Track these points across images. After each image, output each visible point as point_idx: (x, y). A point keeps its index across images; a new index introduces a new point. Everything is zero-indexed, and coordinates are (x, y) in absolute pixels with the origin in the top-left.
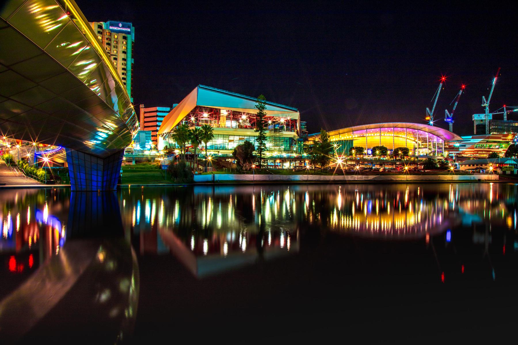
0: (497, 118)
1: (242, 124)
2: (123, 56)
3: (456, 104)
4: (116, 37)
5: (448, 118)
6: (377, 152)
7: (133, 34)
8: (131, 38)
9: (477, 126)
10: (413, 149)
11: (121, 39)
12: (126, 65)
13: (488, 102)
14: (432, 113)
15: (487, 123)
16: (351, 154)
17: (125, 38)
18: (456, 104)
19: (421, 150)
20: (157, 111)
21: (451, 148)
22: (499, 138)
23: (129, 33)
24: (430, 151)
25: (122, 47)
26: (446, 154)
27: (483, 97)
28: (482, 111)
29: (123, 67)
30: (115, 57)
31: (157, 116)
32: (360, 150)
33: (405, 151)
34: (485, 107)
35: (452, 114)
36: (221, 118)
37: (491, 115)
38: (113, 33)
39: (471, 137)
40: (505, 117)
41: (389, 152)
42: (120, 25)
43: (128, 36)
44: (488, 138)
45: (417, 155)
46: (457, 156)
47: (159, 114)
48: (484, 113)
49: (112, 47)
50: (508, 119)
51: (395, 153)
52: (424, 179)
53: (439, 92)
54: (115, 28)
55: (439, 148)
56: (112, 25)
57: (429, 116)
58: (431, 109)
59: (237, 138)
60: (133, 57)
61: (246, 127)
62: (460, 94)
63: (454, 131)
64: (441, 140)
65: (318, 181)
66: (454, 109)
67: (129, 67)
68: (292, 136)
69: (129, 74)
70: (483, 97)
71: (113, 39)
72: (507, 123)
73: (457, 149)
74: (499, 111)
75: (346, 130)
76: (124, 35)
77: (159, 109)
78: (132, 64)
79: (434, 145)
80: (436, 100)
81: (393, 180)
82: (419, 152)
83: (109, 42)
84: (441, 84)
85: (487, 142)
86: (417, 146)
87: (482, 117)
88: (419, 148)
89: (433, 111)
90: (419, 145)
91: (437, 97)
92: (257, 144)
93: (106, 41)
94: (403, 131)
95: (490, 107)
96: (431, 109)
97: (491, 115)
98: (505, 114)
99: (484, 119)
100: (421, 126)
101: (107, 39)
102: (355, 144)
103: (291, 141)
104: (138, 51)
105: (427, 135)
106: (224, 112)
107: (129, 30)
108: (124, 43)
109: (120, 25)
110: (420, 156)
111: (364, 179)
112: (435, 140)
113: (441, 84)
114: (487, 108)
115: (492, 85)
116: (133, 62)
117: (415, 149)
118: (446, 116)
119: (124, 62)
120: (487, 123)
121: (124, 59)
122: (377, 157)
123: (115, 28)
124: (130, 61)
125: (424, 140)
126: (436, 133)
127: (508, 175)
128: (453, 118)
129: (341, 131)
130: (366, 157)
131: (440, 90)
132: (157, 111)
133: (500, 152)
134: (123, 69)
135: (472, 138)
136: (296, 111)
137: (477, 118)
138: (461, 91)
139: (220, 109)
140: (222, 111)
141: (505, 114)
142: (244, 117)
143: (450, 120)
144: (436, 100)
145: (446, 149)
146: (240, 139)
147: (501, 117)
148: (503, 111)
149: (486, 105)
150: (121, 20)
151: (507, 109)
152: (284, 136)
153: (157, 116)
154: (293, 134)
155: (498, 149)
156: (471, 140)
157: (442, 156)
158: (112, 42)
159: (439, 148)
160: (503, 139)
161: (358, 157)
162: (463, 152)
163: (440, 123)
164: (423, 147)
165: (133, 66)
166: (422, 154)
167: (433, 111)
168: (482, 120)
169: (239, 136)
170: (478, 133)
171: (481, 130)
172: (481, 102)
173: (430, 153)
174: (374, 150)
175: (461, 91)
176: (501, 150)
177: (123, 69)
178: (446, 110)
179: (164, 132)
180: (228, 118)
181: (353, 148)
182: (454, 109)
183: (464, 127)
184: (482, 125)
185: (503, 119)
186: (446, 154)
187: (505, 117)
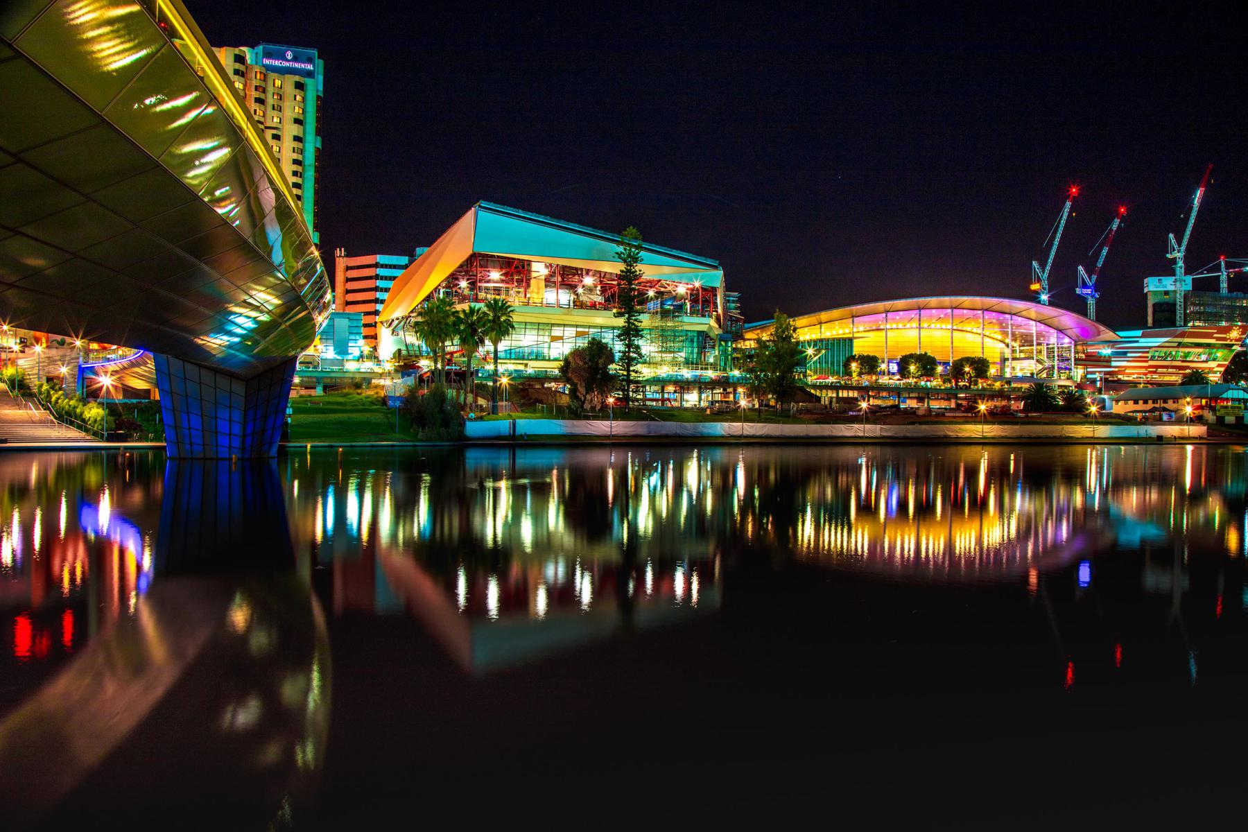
0: (1204, 287)
1: (584, 298)
2: (295, 130)
3: (1105, 251)
4: (278, 83)
5: (1085, 286)
6: (912, 368)
7: (321, 78)
8: (315, 86)
9: (1154, 305)
10: (998, 360)
11: (289, 89)
12: (302, 152)
13: (1183, 248)
14: (1046, 275)
15: (1180, 300)
16: (848, 373)
17: (300, 86)
18: (1105, 251)
19: (1017, 364)
20: (377, 265)
21: (1092, 360)
22: (1209, 336)
23: (310, 74)
24: (1040, 367)
25: (292, 109)
26: (1078, 373)
27: (1171, 236)
28: (1167, 269)
29: (295, 156)
30: (274, 132)
31: (377, 277)
32: (870, 363)
33: (980, 366)
34: (1174, 261)
35: (1094, 277)
36: (533, 282)
37: (1189, 279)
38: (272, 75)
39: (1139, 333)
40: (1224, 285)
41: (940, 369)
42: (289, 55)
43: (308, 81)
44: (1183, 335)
45: (1008, 375)
46: (1106, 380)
47: (382, 272)
48: (1173, 273)
49: (269, 108)
50: (1230, 289)
51: (957, 370)
52: (1025, 434)
53: (1063, 222)
54: (277, 63)
55: (1063, 359)
56: (268, 55)
57: (1039, 280)
58: (1043, 266)
59: (570, 332)
60: (318, 133)
61: (593, 306)
62: (1115, 227)
63: (1101, 319)
64: (1067, 340)
65: (761, 437)
66: (1100, 264)
67: (310, 158)
68: (704, 328)
69: (310, 174)
70: (1171, 236)
71: (270, 90)
72: (1227, 299)
73: (1106, 361)
74: (1209, 271)
75: (836, 313)
76: (297, 78)
77: (381, 259)
78: (317, 150)
79: (1050, 351)
80: (1056, 243)
81: (950, 437)
82: (1013, 368)
83: (262, 96)
84: (1068, 204)
85: (1180, 345)
86: (1008, 354)
87: (1168, 283)
88: (1014, 359)
89: (1048, 268)
90: (1013, 351)
91: (1059, 235)
92: (618, 347)
93: (255, 94)
94: (975, 318)
95: (1186, 260)
96: (1043, 266)
97: (1189, 279)
98: (1224, 276)
99: (1172, 288)
100: (1019, 305)
101: (257, 88)
102: (859, 348)
103: (704, 340)
104: (332, 117)
105: (1033, 328)
106: (539, 269)
107: (310, 67)
108: (298, 98)
109: (289, 55)
110: (1016, 379)
111: (878, 434)
112: (1053, 340)
113: (1068, 204)
114: (1180, 263)
115: (1191, 208)
116: (319, 146)
117: (1004, 360)
118: (1080, 282)
119: (296, 145)
120: (1180, 300)
121: (297, 139)
122: (911, 380)
123: (277, 63)
124: (312, 143)
125: (1027, 340)
126: (1055, 322)
127: (1229, 426)
128: (1096, 287)
129: (824, 316)
130: (884, 380)
131: (1065, 217)
132: (377, 265)
133: (1211, 370)
134: (296, 162)
135: (1143, 336)
136: (715, 267)
137: (1154, 286)
138: (1117, 222)
139: (529, 262)
140: (535, 266)
141: (1224, 276)
142: (589, 281)
143: (1089, 291)
144: (1056, 243)
145: (1078, 361)
146: (579, 335)
147: (1213, 285)
148: (1219, 270)
149: (1178, 254)
150: (290, 43)
151: (1228, 266)
152: (686, 328)
153: (377, 277)
154: (708, 323)
155: (1206, 362)
156: (1141, 340)
157: (1069, 378)
158: (270, 95)
159: (1063, 359)
160: (1218, 339)
161: (866, 380)
162: (1122, 370)
163: (1065, 299)
164: (1022, 355)
165: (320, 155)
166: (1020, 374)
167: (1048, 268)
168: (1166, 293)
169: (577, 326)
170: (1156, 324)
171: (1166, 317)
172: (1165, 248)
173: (1041, 371)
174: (903, 364)
175: (1117, 222)
176: (1212, 364)
177: (296, 162)
178: (1080, 268)
179: (394, 316)
180: (548, 282)
181: (852, 358)
182: (1100, 264)
183: (1124, 309)
184: (1167, 304)
185: (1218, 289)
186: (1078, 373)
187: (1224, 285)
